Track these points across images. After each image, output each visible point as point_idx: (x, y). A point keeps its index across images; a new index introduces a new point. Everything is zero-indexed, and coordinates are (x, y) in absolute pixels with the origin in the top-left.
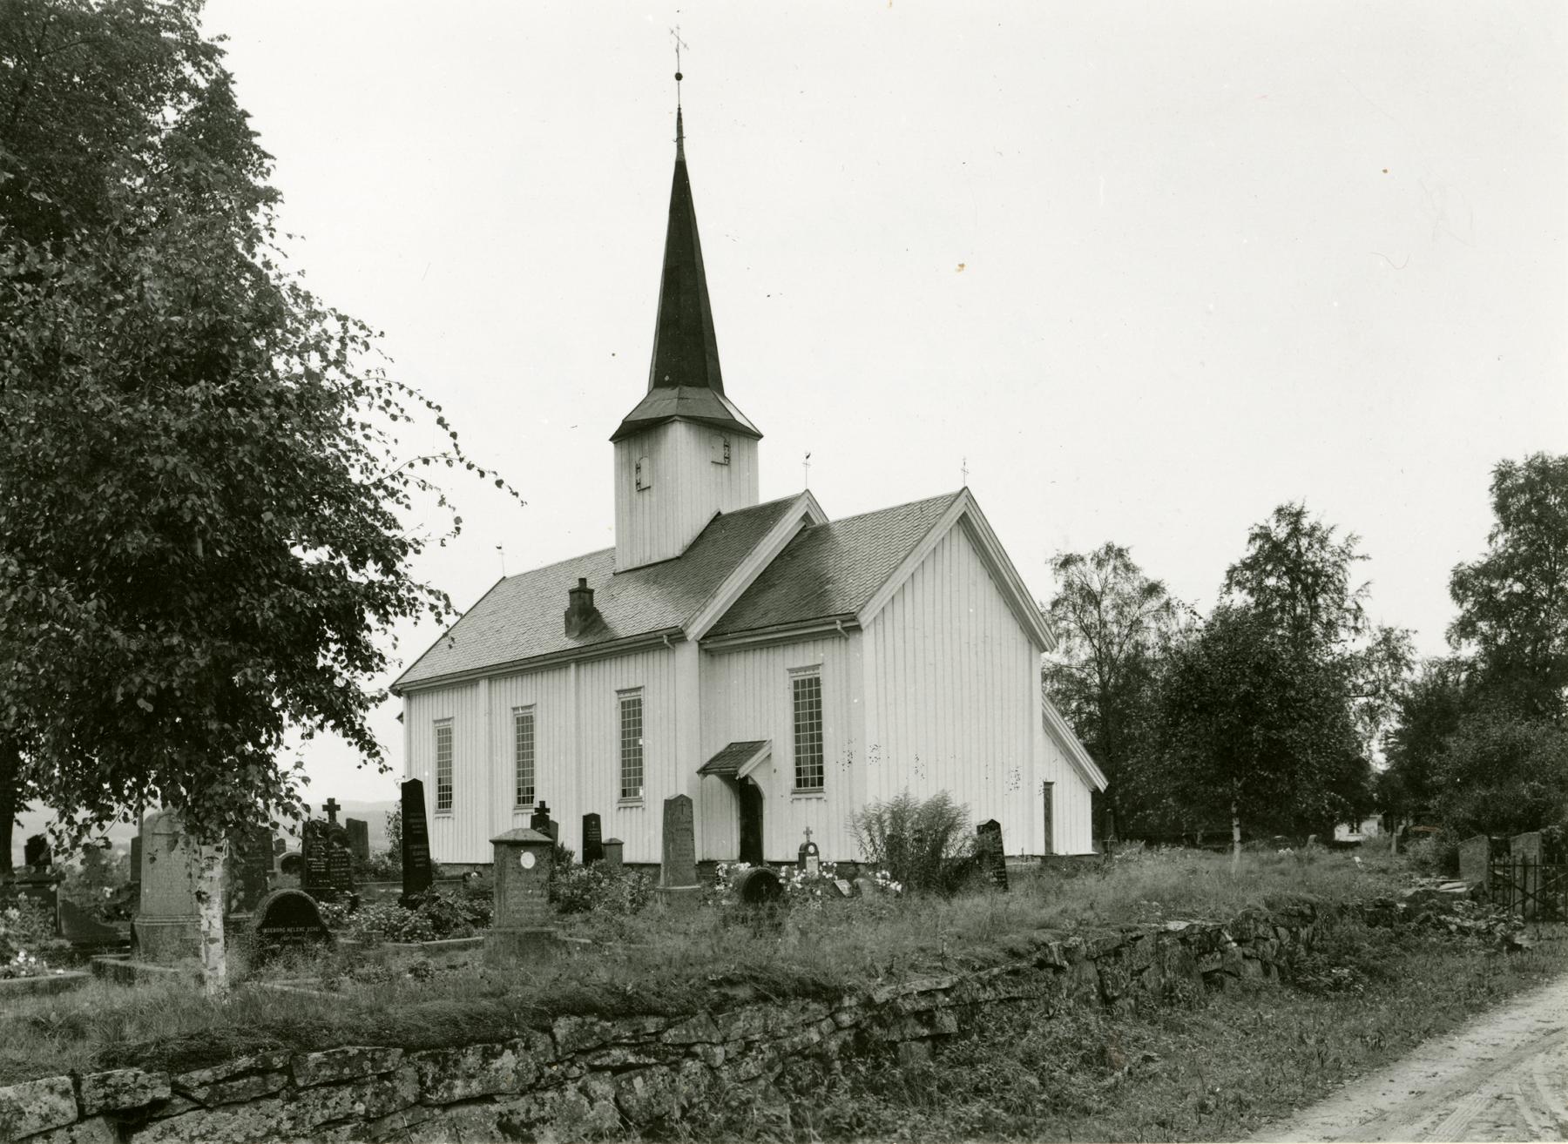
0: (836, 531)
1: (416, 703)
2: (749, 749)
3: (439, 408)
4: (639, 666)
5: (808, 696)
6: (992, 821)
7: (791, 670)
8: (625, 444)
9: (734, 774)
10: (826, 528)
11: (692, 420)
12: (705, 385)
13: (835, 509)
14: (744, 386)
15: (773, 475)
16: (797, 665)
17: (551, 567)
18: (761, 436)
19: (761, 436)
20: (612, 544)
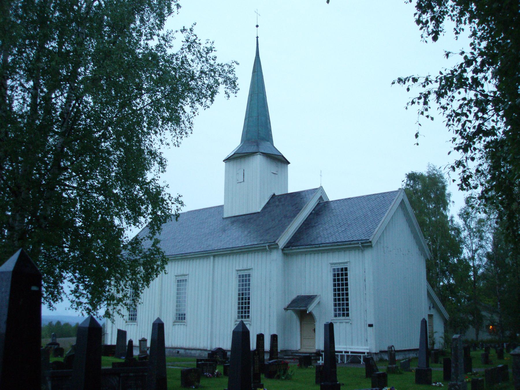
0: (333, 206)
1: (216, 259)
2: (310, 299)
3: (408, 104)
4: (256, 256)
5: (341, 278)
6: (144, 338)
7: (332, 264)
8: (228, 163)
9: (301, 309)
10: (328, 202)
11: (264, 154)
12: (268, 141)
13: (332, 196)
14: (281, 141)
15: (296, 181)
16: (335, 262)
17: (359, 197)
18: (289, 163)
19: (289, 163)
20: (222, 203)
